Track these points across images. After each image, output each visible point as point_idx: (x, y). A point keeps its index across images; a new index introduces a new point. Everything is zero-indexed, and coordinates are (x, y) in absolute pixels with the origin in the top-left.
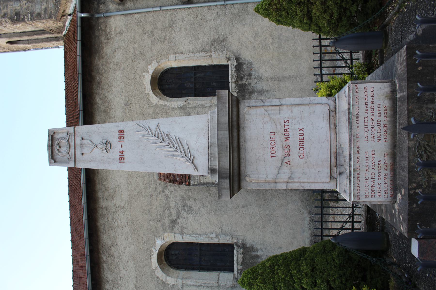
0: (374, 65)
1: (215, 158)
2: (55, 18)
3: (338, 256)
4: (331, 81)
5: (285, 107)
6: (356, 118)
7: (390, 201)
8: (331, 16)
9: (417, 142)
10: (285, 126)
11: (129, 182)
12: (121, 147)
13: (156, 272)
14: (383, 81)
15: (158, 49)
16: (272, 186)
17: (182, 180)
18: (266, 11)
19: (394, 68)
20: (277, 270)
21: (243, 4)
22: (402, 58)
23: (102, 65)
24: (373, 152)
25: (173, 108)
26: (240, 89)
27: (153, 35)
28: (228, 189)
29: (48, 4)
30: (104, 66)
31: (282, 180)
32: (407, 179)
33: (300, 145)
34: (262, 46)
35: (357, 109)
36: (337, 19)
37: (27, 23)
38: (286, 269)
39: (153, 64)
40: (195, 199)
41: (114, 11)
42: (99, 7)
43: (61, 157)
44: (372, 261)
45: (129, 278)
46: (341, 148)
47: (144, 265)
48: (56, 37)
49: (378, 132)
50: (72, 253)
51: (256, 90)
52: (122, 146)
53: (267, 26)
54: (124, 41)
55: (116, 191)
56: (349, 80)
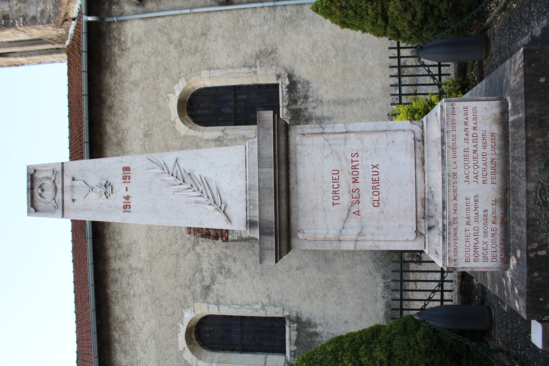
0: (470, 82)
1: (255, 206)
2: (54, 23)
3: (424, 338)
4: (414, 103)
5: (352, 135)
6: (451, 150)
7: (500, 266)
8: (414, 16)
9: (539, 184)
10: (352, 161)
11: (149, 236)
12: (127, 190)
13: (184, 355)
14: (489, 98)
15: (187, 64)
16: (334, 246)
17: (217, 234)
18: (327, 9)
19: (505, 80)
20: (342, 356)
21: (298, 6)
22: (517, 66)
23: (115, 84)
24: (476, 199)
25: (207, 140)
26: (293, 115)
27: (181, 45)
28: (273, 250)
29: (46, 5)
30: (117, 86)
31: (349, 237)
32: (524, 236)
33: (374, 188)
34: (322, 59)
35: (454, 137)
36: (421, 20)
37: (18, 29)
38: (354, 355)
39: (180, 83)
40: (235, 259)
41: (131, 13)
42: (111, 8)
43: (45, 204)
44: (471, 346)
45: (149, 362)
46: (431, 192)
47: (168, 345)
48: (57, 49)
49: (483, 170)
50: (77, 329)
51: (314, 116)
52: (128, 189)
53: (328, 34)
54: (144, 53)
55: (132, 248)
56: (437, 101)
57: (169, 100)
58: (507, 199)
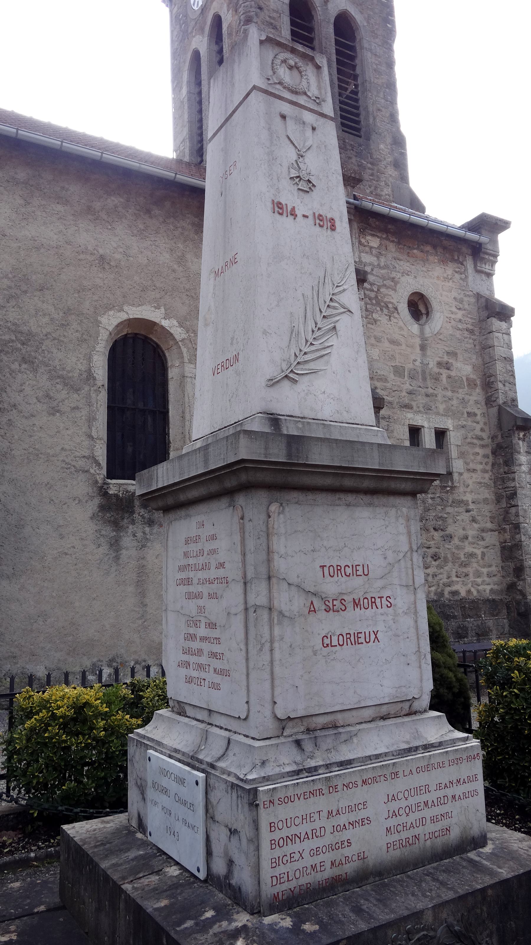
6: (426, 764)
23: (183, 228)
24: (366, 821)
25: (90, 358)
26: (124, 500)
30: (180, 230)
35: (441, 765)
39: (179, 330)
46: (351, 737)
57: (156, 308)
58: (367, 879)
